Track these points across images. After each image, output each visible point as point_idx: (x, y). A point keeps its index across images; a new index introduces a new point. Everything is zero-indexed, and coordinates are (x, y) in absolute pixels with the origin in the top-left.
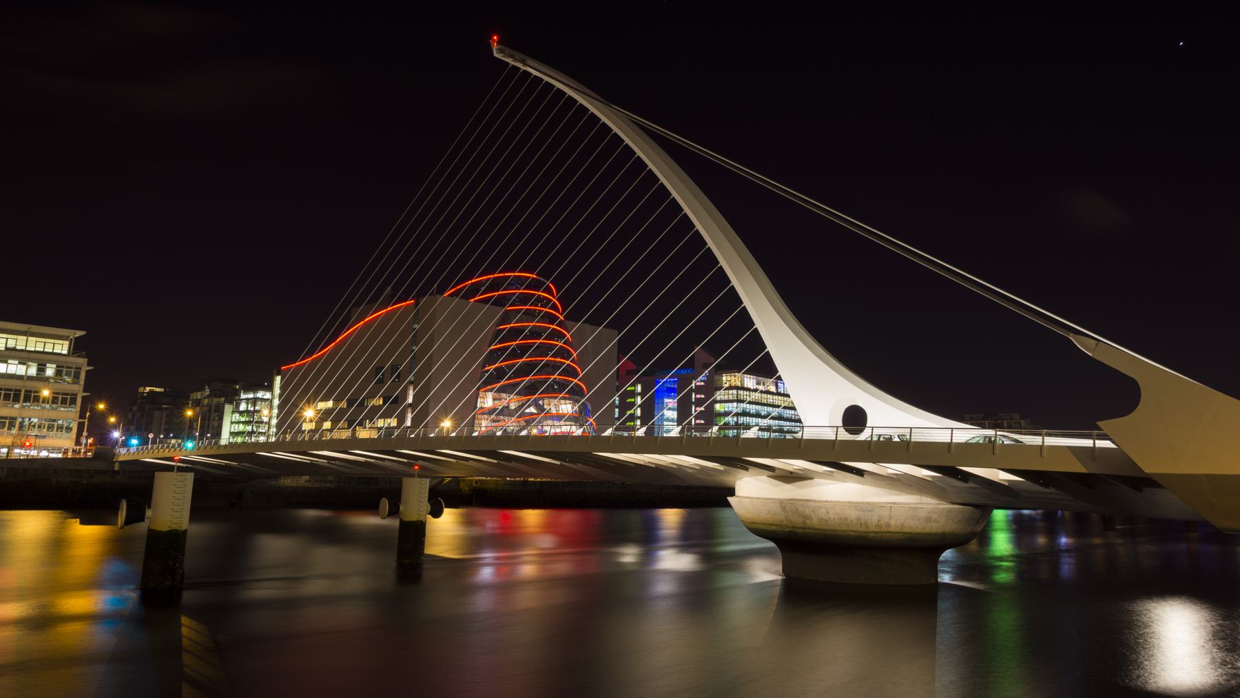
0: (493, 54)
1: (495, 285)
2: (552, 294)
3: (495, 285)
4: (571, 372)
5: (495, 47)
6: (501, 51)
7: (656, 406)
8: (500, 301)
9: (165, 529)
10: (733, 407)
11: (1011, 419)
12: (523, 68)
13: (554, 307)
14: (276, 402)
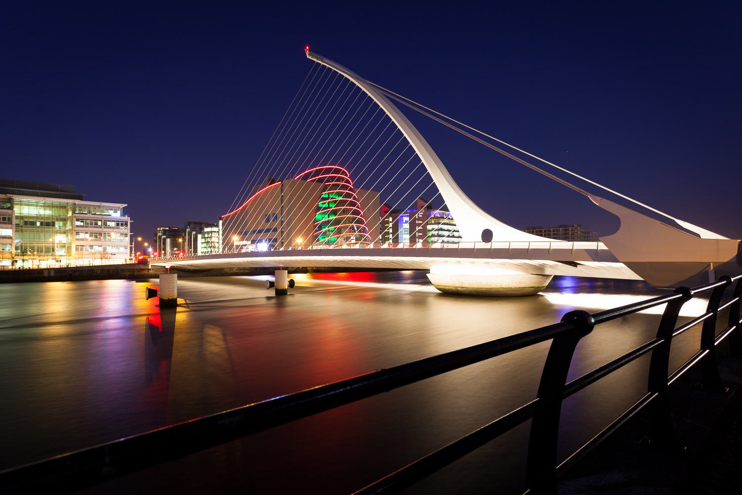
0: (306, 57)
1: (318, 173)
2: (347, 175)
3: (318, 173)
4: (356, 213)
5: (307, 55)
6: (310, 55)
7: (399, 227)
8: (320, 180)
9: (167, 299)
10: (436, 227)
11: (573, 226)
12: (322, 63)
13: (347, 181)
14: (221, 232)
